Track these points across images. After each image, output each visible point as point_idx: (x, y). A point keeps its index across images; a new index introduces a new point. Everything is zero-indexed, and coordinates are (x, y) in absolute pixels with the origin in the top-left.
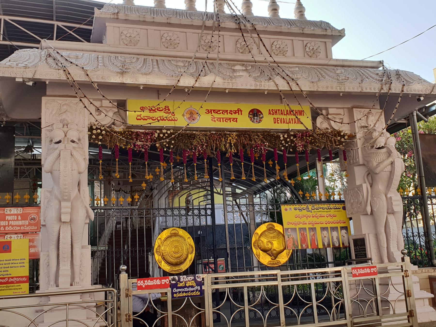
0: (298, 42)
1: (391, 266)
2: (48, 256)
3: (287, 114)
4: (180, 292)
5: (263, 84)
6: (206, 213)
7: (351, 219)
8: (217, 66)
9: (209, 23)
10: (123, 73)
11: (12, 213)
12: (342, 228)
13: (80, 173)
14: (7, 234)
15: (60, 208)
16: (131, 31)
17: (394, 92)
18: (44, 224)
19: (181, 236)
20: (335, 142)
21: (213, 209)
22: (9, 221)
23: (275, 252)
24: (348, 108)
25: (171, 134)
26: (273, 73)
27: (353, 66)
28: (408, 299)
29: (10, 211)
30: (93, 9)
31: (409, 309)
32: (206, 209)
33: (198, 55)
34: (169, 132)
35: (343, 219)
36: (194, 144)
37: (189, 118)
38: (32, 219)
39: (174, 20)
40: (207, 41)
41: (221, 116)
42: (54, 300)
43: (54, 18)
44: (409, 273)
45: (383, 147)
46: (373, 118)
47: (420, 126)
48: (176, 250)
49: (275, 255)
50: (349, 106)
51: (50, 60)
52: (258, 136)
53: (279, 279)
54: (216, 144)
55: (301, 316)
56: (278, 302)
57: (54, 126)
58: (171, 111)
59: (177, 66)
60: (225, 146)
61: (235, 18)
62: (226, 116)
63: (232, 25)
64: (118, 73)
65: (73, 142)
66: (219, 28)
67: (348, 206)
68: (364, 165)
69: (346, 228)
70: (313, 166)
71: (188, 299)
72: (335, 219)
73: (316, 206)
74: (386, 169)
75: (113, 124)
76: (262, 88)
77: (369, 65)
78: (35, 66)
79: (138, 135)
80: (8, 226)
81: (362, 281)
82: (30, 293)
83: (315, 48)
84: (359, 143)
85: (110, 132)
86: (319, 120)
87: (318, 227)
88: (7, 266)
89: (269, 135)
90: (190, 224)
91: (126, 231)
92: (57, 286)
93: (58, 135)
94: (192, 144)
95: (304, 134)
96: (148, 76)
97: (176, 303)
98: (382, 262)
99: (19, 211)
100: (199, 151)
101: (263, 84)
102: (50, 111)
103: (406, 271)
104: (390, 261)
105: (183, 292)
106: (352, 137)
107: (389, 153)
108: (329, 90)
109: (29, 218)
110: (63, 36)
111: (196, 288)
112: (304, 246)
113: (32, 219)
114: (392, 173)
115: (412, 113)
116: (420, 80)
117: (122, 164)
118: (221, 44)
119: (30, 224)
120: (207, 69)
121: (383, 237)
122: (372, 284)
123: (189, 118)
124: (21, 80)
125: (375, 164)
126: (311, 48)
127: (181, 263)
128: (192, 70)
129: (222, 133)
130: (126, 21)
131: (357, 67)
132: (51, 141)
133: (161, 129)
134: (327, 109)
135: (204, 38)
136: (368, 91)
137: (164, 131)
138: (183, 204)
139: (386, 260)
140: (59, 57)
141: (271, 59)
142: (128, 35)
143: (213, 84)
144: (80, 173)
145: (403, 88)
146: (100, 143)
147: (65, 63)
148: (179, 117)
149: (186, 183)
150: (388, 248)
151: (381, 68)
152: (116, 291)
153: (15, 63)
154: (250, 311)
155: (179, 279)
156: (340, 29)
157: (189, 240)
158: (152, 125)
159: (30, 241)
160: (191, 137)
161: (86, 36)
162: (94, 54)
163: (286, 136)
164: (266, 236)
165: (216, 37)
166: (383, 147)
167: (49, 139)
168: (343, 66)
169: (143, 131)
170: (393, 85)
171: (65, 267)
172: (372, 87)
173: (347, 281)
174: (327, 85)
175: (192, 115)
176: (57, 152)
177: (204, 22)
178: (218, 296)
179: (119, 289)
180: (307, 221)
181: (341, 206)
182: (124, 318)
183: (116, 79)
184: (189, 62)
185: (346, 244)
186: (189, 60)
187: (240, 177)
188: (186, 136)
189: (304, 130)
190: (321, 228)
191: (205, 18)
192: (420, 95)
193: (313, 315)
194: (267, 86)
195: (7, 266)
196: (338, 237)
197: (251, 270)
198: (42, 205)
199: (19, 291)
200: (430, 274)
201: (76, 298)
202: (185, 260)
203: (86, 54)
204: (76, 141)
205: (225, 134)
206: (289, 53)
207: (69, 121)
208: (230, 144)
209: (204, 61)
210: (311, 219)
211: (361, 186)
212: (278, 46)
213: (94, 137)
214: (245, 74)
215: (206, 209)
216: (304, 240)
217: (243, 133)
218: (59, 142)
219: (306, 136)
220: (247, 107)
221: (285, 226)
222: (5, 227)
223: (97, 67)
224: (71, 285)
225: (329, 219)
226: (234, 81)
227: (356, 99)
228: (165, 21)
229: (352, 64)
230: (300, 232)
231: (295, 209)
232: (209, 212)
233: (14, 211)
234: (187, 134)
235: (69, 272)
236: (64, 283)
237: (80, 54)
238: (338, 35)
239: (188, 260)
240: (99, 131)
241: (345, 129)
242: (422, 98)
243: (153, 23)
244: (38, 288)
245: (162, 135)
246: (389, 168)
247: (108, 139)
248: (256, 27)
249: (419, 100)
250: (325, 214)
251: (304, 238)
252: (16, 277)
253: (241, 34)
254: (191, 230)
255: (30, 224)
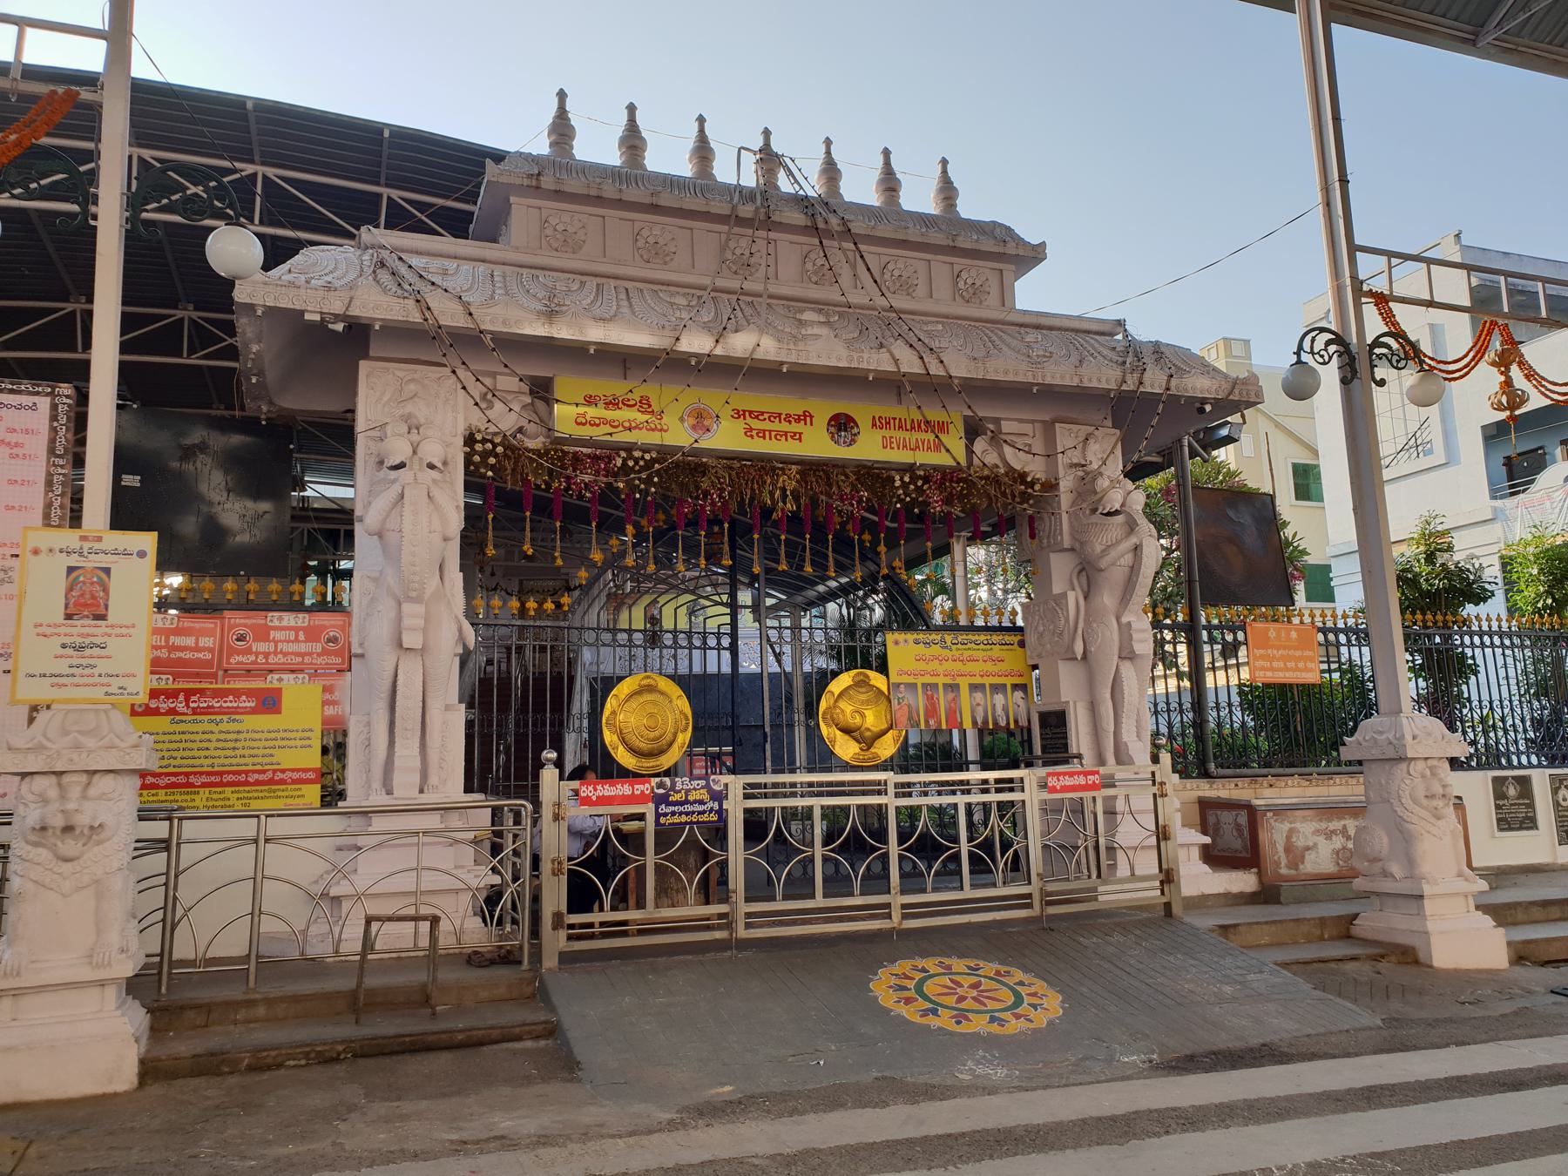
0: (941, 267)
1: (1121, 773)
2: (368, 724)
3: (913, 428)
4: (673, 814)
5: (866, 356)
6: (719, 643)
7: (1035, 667)
8: (763, 310)
9: (746, 211)
10: (551, 315)
11: (285, 623)
12: (1015, 687)
13: (446, 539)
14: (271, 671)
15: (399, 618)
16: (566, 218)
17: (1149, 390)
18: (359, 651)
19: (662, 693)
20: (1014, 497)
21: (734, 636)
22: (276, 643)
23: (868, 734)
24: (1043, 422)
25: (653, 461)
26: (888, 333)
27: (1059, 329)
28: (1163, 844)
29: (280, 619)
30: (483, 165)
31: (1164, 866)
32: (718, 635)
33: (720, 283)
34: (647, 457)
35: (1019, 666)
36: (704, 486)
37: (694, 427)
38: (329, 640)
39: (666, 200)
40: (738, 252)
41: (767, 425)
42: (379, 823)
43: (383, 181)
44: (1168, 788)
45: (1117, 513)
46: (1097, 446)
47: (1193, 466)
48: (652, 723)
49: (867, 740)
50: (1047, 418)
51: (384, 276)
52: (847, 476)
53: (891, 790)
54: (753, 489)
55: (937, 874)
56: (886, 842)
57: (389, 430)
58: (655, 407)
59: (672, 304)
60: (772, 494)
61: (802, 202)
62: (776, 426)
63: (798, 218)
64: (540, 313)
65: (431, 466)
66: (769, 224)
67: (1031, 639)
68: (1072, 550)
69: (1023, 687)
70: (944, 550)
71: (691, 829)
72: (999, 667)
73: (962, 637)
74: (1122, 561)
75: (520, 430)
76: (864, 366)
77: (1094, 327)
78: (352, 286)
79: (577, 459)
80: (276, 653)
81: (1067, 803)
82: (323, 806)
83: (978, 283)
84: (1065, 499)
85: (513, 451)
86: (980, 445)
87: (964, 683)
88: (271, 743)
89: (872, 475)
90: (683, 669)
91: (505, 682)
92: (389, 793)
93: (399, 449)
94: (697, 488)
95: (944, 477)
96: (610, 326)
97: (665, 837)
98: (1102, 761)
99: (301, 619)
100: (713, 503)
101: (866, 356)
102: (377, 396)
103: (1162, 784)
104: (1119, 762)
105: (681, 814)
106: (1051, 486)
107: (1131, 526)
108: (1010, 378)
109: (324, 637)
110: (399, 219)
111: (710, 805)
112: (932, 722)
113: (329, 640)
114: (1134, 569)
115: (1180, 441)
116: (1207, 369)
117: (503, 529)
118: (771, 260)
119: (325, 652)
120: (738, 313)
121: (1107, 709)
122: (1078, 809)
123: (694, 427)
124: (317, 318)
125: (1098, 548)
126: (969, 281)
127: (662, 752)
128: (707, 316)
129: (766, 466)
130: (559, 195)
131: (1067, 330)
132: (381, 463)
133: (629, 448)
134: (997, 421)
135: (732, 244)
136: (1094, 384)
137: (637, 454)
138: (639, 623)
139: (1111, 759)
140: (403, 270)
141: (882, 302)
142: (560, 228)
143: (754, 350)
144: (446, 539)
145: (1168, 382)
146: (490, 473)
147: (419, 285)
148: (670, 425)
149: (649, 577)
150: (1117, 734)
151: (1120, 337)
152: (530, 807)
153: (303, 278)
154: (825, 859)
155: (673, 784)
156: (1035, 242)
157: (679, 702)
158: (615, 438)
159: (326, 689)
160: (701, 469)
161: (457, 225)
162: (482, 267)
163: (907, 479)
164: (851, 698)
165: (761, 244)
166: (1117, 513)
167: (374, 459)
168: (1038, 327)
169: (589, 450)
170: (1147, 375)
171: (407, 751)
172: (1102, 376)
173: (1036, 802)
174: (1006, 367)
175: (701, 419)
176: (397, 488)
177: (734, 208)
178: (755, 826)
179: (537, 804)
180: (940, 670)
181: (1015, 639)
182: (546, 867)
183: (537, 329)
184: (699, 297)
185: (1023, 722)
186: (699, 293)
187: (800, 568)
188: (685, 469)
189: (950, 467)
190: (971, 685)
191: (736, 199)
192: (1204, 401)
193: (960, 873)
194: (877, 362)
195: (271, 743)
196: (1007, 708)
197: (793, 771)
198: (355, 609)
199: (297, 801)
200: (1201, 794)
201: (432, 821)
202: (670, 744)
203: (466, 267)
204: (439, 465)
205: (774, 469)
206: (921, 291)
207: (422, 420)
208: (784, 490)
209: (735, 297)
210: (949, 666)
211: (1064, 595)
212: (896, 273)
213: (477, 458)
214: (823, 331)
215: (718, 635)
216: (931, 711)
217: (813, 469)
218: (401, 466)
219: (951, 481)
220: (824, 409)
221: (894, 678)
222: (266, 655)
223: (492, 298)
224: (421, 791)
225: (989, 667)
226: (801, 346)
227: (1063, 402)
228: (647, 200)
229: (1057, 323)
230: (924, 693)
231: (917, 642)
232: (726, 642)
233: (289, 619)
234: (689, 464)
235: (418, 763)
236: (406, 787)
237: (452, 265)
238: (1031, 256)
239: (675, 746)
240: (489, 446)
241: (1035, 468)
242: (1208, 408)
243: (620, 204)
244: (342, 795)
245: (631, 463)
246: (1128, 559)
247: (509, 466)
248: (851, 225)
249: (1201, 411)
250: (980, 654)
251: (933, 705)
252: (293, 770)
253: (816, 241)
254: (686, 683)
255: (325, 652)
